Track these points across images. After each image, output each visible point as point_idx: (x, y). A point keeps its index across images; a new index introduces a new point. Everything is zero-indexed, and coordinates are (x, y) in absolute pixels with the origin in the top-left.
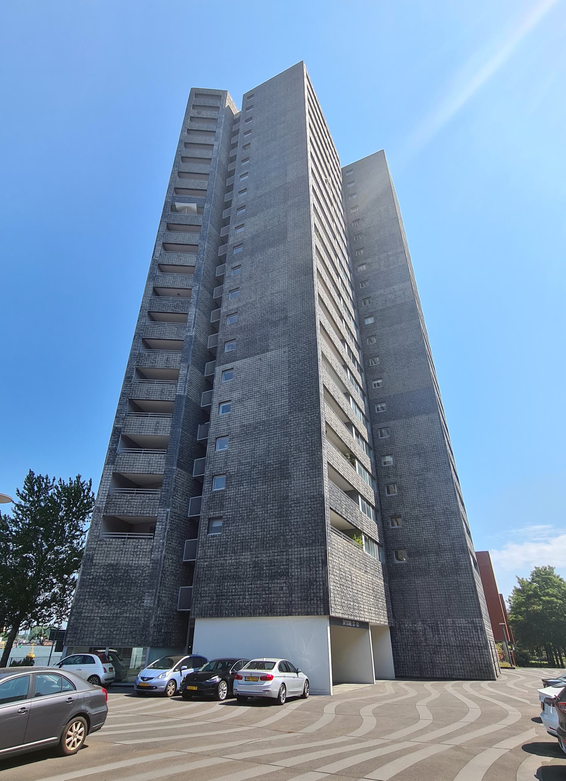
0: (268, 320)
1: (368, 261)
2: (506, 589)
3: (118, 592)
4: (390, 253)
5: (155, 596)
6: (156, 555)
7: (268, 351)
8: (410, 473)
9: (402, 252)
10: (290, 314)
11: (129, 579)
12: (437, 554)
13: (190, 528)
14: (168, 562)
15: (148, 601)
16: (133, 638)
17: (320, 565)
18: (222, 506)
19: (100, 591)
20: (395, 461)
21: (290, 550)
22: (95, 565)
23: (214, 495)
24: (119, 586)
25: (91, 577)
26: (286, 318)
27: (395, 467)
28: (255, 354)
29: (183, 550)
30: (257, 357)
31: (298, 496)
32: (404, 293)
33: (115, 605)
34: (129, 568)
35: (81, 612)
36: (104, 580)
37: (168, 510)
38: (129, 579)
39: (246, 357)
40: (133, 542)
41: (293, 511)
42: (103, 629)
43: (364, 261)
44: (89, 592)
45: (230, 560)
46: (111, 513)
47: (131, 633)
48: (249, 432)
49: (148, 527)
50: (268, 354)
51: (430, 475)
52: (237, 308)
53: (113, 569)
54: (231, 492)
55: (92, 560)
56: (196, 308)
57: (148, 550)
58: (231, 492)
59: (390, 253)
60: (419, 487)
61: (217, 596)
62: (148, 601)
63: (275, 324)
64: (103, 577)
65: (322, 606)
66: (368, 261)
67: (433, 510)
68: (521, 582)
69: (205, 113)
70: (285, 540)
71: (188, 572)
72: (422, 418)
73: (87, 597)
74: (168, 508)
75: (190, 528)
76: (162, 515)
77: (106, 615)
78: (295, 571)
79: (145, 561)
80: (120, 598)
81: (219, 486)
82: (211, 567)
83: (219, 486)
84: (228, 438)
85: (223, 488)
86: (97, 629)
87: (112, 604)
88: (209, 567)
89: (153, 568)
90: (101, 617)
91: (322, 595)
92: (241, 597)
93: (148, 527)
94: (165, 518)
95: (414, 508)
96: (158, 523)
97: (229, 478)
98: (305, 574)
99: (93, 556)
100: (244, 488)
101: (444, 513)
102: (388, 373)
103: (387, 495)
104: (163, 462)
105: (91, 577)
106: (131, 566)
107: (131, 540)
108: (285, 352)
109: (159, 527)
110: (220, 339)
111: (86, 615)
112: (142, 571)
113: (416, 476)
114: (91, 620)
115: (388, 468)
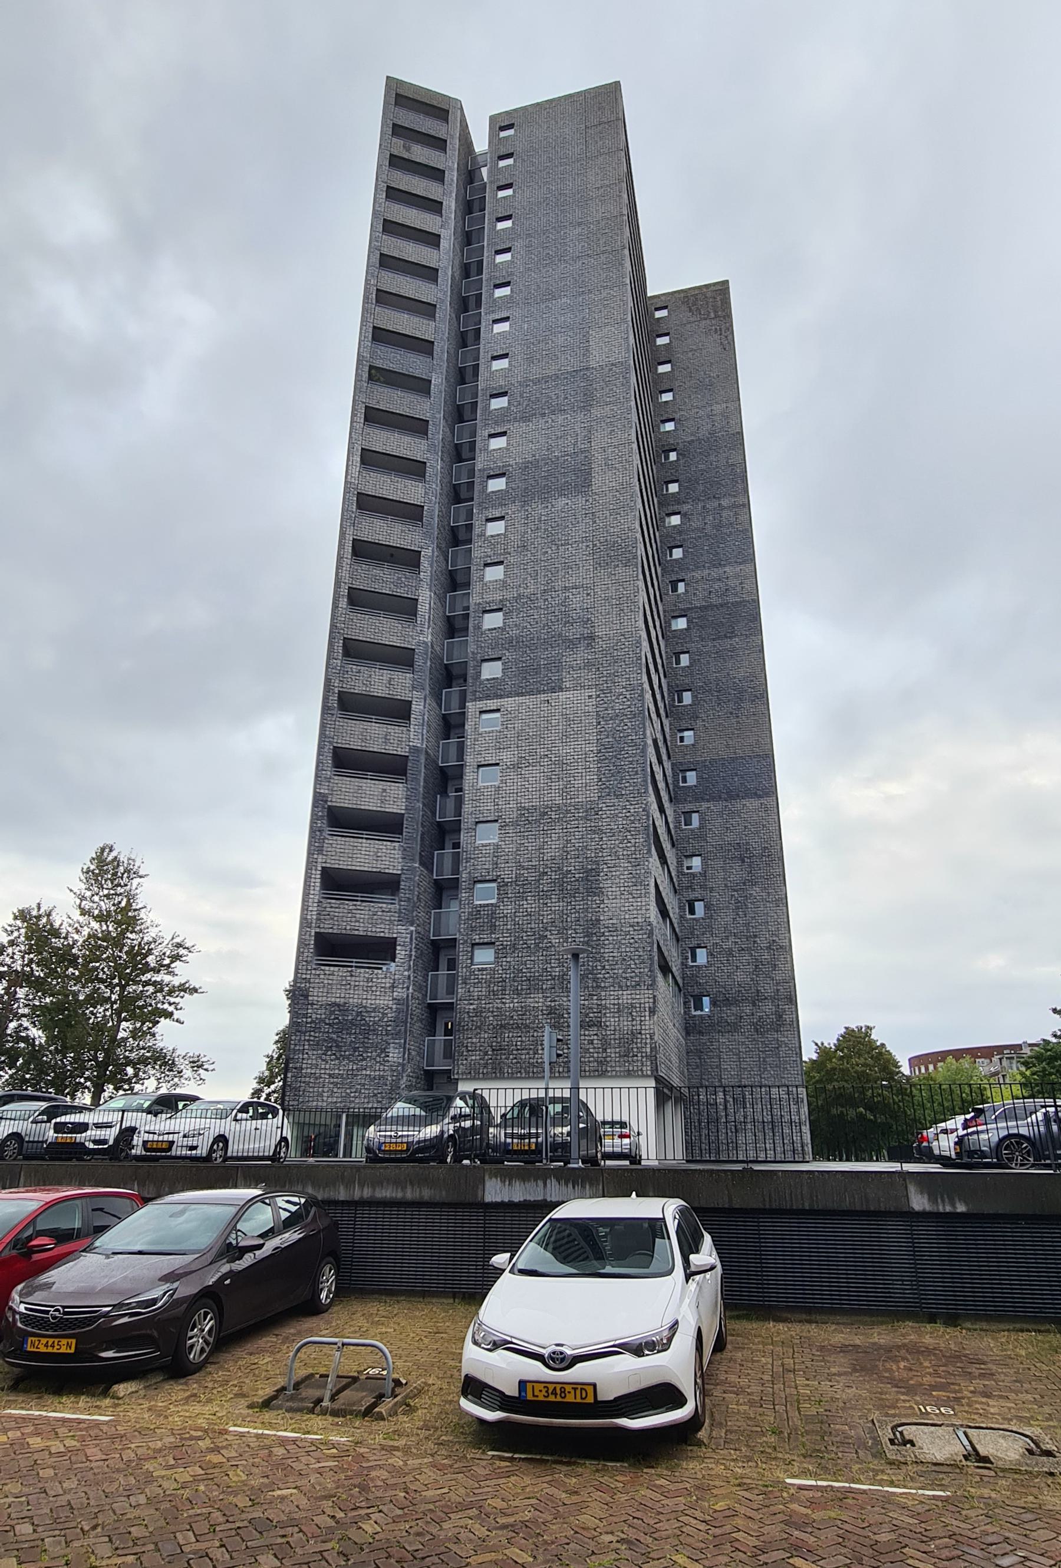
0: (560, 635)
1: (685, 508)
2: (809, 1053)
3: (352, 1042)
4: (725, 502)
5: (404, 1048)
6: (400, 993)
7: (561, 689)
8: (726, 886)
9: (744, 505)
10: (599, 632)
11: (364, 1025)
12: (754, 1005)
13: (438, 952)
14: (413, 1004)
15: (394, 1055)
16: (378, 1102)
17: (647, 1014)
18: (493, 928)
19: (325, 1040)
20: (704, 863)
21: (603, 993)
22: (312, 1004)
23: (478, 911)
24: (351, 1034)
25: (309, 1020)
26: (592, 638)
27: (704, 874)
28: (539, 692)
29: (426, 987)
30: (543, 697)
31: (615, 921)
32: (741, 583)
33: (348, 1059)
34: (362, 1012)
35: (302, 1069)
36: (329, 1024)
37: (412, 928)
38: (364, 1025)
39: (522, 694)
40: (365, 972)
41: (606, 942)
42: (335, 1090)
43: (676, 508)
44: (308, 1040)
45: (511, 1003)
46: (327, 928)
47: (375, 1095)
48: (533, 819)
49: (380, 950)
50: (563, 696)
51: (755, 891)
52: (501, 601)
53: (340, 1011)
54: (508, 909)
55: (306, 997)
56: (431, 591)
57: (388, 985)
58: (508, 909)
59: (725, 502)
60: (738, 908)
61: (493, 1050)
62: (394, 1055)
63: (571, 644)
64: (327, 1021)
65: (649, 1063)
66: (685, 508)
67: (755, 942)
68: (883, 1045)
69: (420, 154)
70: (595, 980)
71: (435, 1014)
72: (752, 804)
73: (306, 1047)
74: (412, 925)
75: (438, 952)
76: (404, 934)
77: (337, 1071)
78: (611, 1021)
79: (385, 1001)
80: (355, 1049)
81: (485, 895)
82: (481, 1012)
83: (485, 895)
84: (497, 825)
85: (493, 901)
86: (326, 1090)
87: (344, 1057)
88: (478, 1012)
89: (398, 1011)
90: (330, 1075)
91: (648, 1050)
92: (531, 1052)
93: (380, 950)
94: (408, 940)
95: (727, 937)
96: (398, 948)
97: (503, 886)
98: (626, 1024)
99: (307, 990)
100: (530, 904)
101: (769, 948)
102: (704, 721)
103: (689, 916)
104: (398, 854)
105: (309, 1020)
106: (365, 1007)
107: (362, 970)
108: (590, 697)
109: (401, 952)
110: (473, 653)
111: (309, 1071)
112: (383, 1013)
113: (735, 890)
114: (316, 1078)
115: (693, 875)
